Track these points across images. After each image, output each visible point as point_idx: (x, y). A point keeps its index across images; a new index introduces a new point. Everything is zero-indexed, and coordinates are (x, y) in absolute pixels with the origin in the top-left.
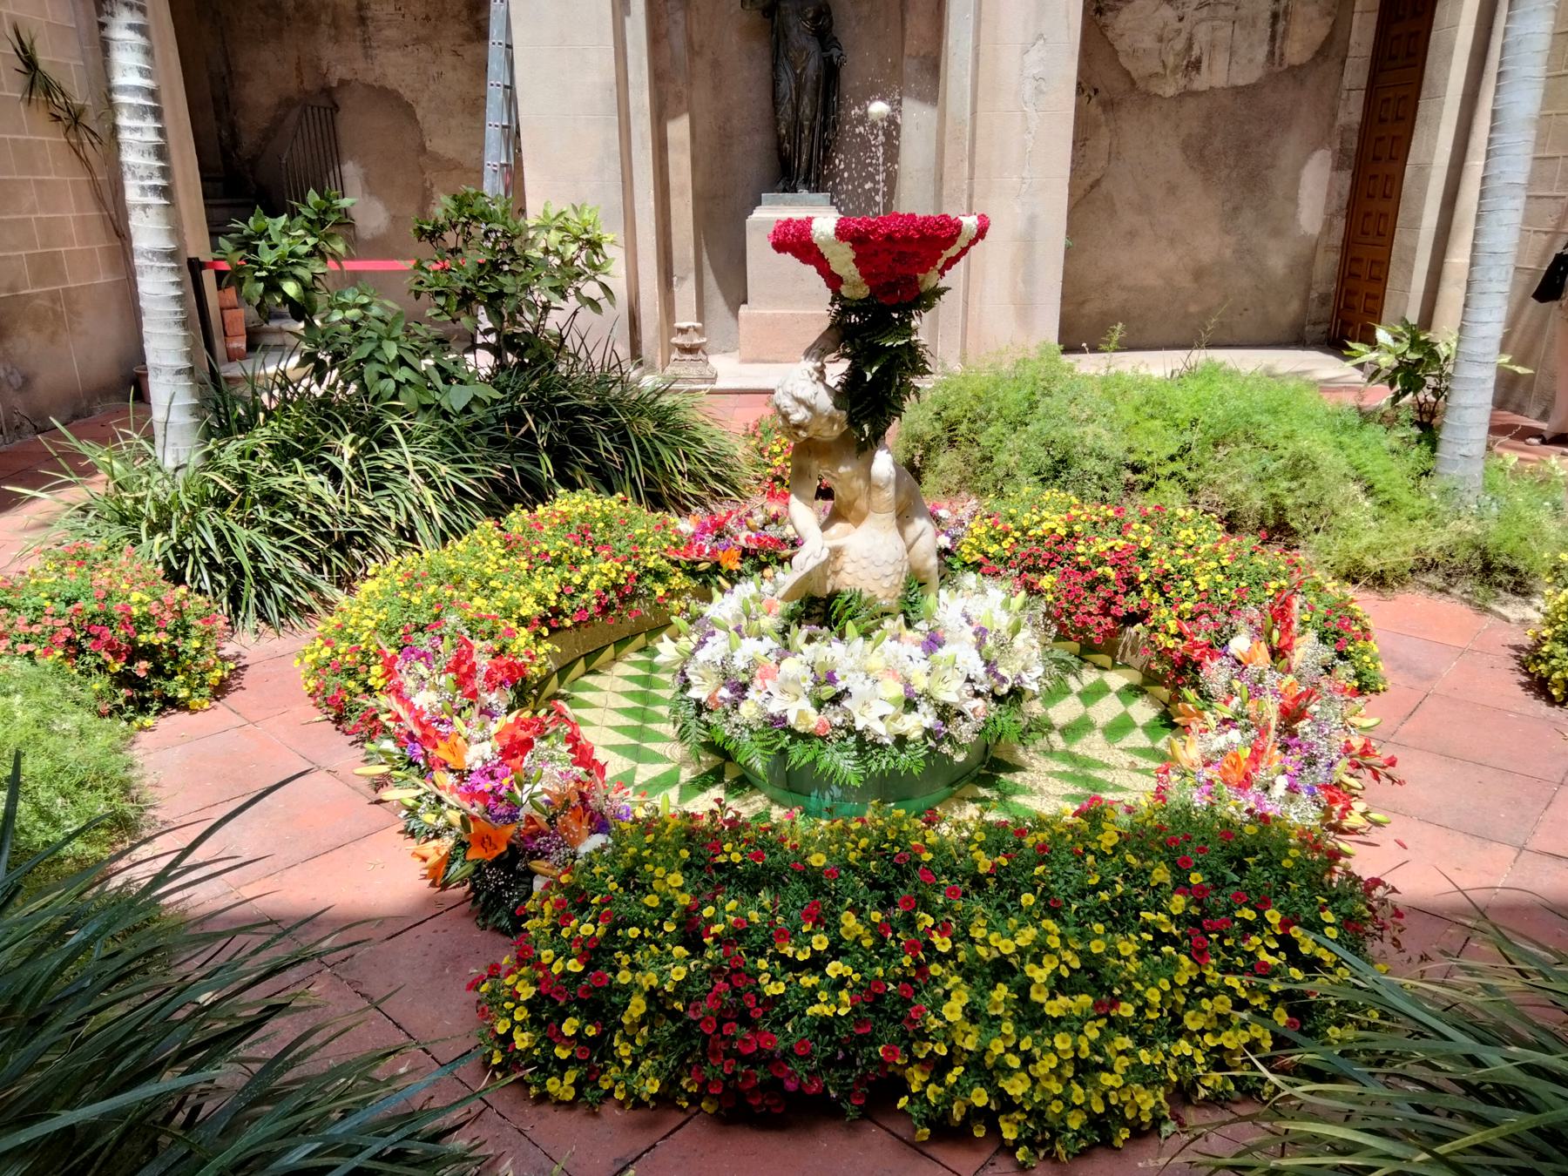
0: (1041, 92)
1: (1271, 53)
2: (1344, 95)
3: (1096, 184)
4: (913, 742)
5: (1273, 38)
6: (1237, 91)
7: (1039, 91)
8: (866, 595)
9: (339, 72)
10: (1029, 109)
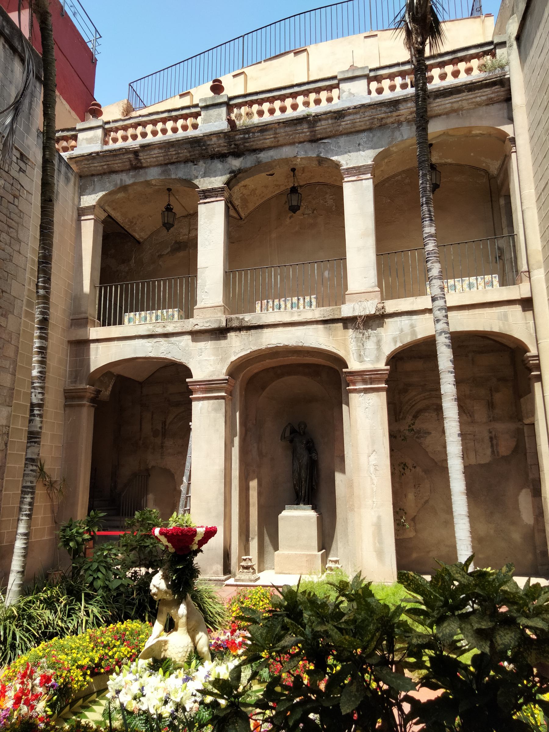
0: (377, 470)
1: (493, 452)
2: (529, 467)
3: (427, 502)
4: (165, 718)
5: (492, 446)
6: (481, 466)
7: (376, 470)
8: (173, 660)
9: (152, 464)
10: (373, 476)
